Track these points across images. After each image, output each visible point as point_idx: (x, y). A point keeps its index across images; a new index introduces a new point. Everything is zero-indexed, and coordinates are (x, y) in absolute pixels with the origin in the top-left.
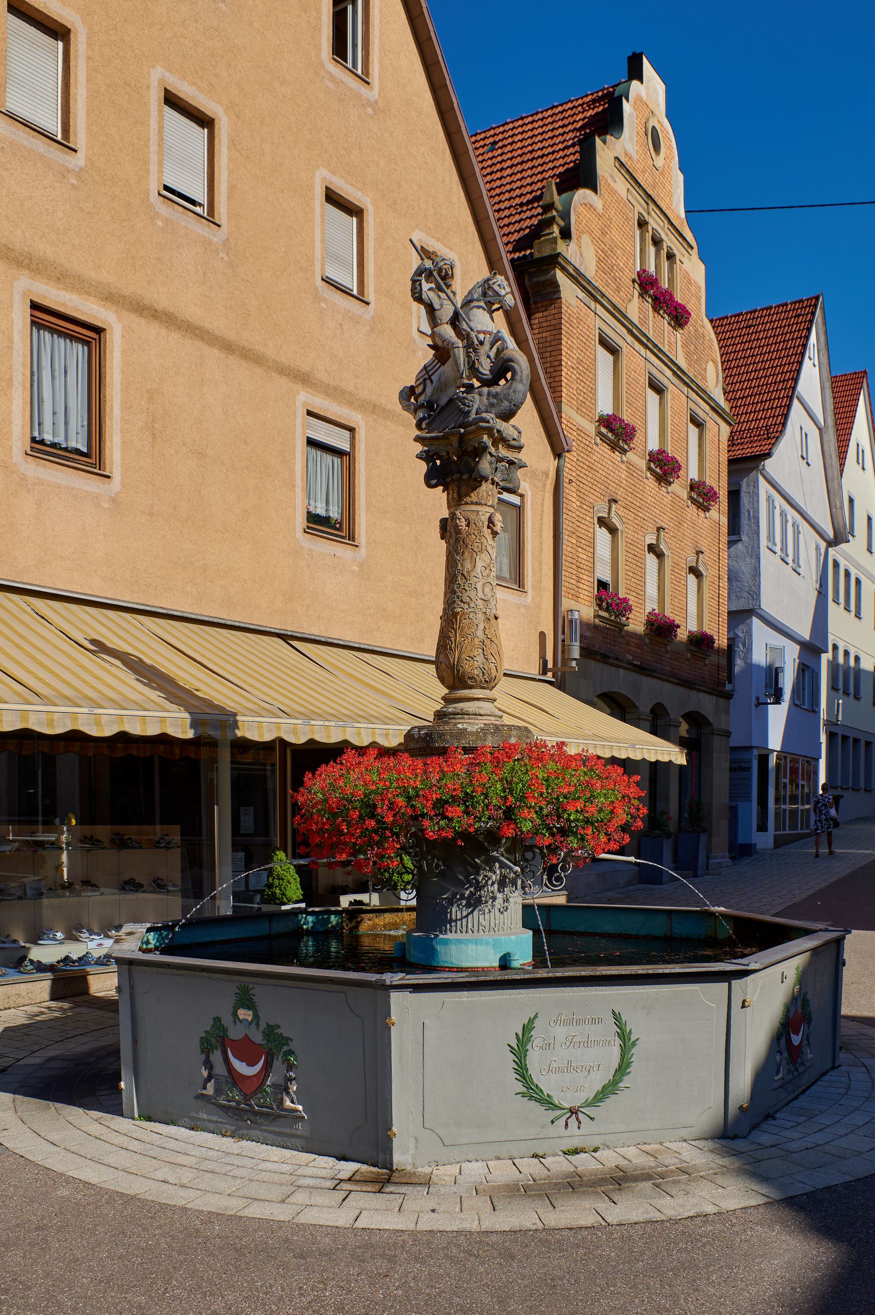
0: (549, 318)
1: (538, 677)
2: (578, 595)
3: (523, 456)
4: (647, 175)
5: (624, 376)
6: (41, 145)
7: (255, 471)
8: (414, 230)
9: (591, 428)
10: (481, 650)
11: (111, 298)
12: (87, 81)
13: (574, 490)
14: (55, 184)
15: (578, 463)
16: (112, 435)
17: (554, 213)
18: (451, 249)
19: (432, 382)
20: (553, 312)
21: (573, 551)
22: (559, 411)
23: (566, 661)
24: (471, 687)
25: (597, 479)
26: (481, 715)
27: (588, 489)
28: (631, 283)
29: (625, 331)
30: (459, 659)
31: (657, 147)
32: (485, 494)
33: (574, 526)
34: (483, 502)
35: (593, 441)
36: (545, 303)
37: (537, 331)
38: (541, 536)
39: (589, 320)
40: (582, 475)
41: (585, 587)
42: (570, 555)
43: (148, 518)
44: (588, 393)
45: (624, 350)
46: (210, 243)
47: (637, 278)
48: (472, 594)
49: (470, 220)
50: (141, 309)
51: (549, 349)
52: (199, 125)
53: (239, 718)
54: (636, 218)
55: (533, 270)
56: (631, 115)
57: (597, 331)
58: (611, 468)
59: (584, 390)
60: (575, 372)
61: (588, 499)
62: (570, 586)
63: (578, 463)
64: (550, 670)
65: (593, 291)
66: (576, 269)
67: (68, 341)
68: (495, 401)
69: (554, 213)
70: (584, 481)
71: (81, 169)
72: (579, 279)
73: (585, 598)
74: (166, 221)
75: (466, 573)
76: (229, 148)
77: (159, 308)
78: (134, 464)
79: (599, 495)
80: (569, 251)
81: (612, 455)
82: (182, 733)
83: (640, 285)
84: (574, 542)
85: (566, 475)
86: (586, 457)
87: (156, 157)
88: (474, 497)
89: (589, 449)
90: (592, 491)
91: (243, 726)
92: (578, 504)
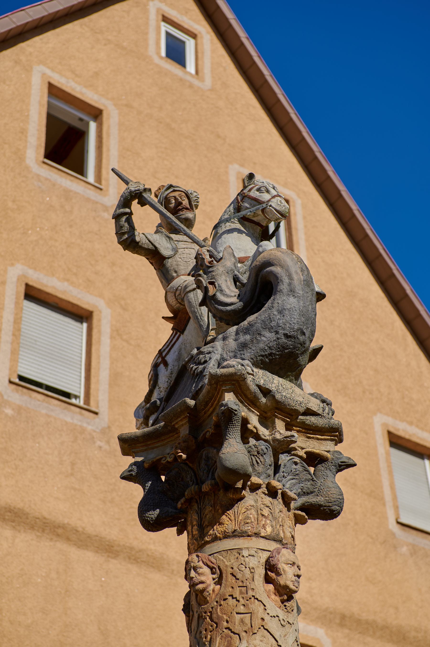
3: (345, 450)
32: (253, 514)
34: (248, 528)
46: (83, 431)
68: (248, 337)
74: (19, 409)
76: (112, 338)
88: (228, 522)
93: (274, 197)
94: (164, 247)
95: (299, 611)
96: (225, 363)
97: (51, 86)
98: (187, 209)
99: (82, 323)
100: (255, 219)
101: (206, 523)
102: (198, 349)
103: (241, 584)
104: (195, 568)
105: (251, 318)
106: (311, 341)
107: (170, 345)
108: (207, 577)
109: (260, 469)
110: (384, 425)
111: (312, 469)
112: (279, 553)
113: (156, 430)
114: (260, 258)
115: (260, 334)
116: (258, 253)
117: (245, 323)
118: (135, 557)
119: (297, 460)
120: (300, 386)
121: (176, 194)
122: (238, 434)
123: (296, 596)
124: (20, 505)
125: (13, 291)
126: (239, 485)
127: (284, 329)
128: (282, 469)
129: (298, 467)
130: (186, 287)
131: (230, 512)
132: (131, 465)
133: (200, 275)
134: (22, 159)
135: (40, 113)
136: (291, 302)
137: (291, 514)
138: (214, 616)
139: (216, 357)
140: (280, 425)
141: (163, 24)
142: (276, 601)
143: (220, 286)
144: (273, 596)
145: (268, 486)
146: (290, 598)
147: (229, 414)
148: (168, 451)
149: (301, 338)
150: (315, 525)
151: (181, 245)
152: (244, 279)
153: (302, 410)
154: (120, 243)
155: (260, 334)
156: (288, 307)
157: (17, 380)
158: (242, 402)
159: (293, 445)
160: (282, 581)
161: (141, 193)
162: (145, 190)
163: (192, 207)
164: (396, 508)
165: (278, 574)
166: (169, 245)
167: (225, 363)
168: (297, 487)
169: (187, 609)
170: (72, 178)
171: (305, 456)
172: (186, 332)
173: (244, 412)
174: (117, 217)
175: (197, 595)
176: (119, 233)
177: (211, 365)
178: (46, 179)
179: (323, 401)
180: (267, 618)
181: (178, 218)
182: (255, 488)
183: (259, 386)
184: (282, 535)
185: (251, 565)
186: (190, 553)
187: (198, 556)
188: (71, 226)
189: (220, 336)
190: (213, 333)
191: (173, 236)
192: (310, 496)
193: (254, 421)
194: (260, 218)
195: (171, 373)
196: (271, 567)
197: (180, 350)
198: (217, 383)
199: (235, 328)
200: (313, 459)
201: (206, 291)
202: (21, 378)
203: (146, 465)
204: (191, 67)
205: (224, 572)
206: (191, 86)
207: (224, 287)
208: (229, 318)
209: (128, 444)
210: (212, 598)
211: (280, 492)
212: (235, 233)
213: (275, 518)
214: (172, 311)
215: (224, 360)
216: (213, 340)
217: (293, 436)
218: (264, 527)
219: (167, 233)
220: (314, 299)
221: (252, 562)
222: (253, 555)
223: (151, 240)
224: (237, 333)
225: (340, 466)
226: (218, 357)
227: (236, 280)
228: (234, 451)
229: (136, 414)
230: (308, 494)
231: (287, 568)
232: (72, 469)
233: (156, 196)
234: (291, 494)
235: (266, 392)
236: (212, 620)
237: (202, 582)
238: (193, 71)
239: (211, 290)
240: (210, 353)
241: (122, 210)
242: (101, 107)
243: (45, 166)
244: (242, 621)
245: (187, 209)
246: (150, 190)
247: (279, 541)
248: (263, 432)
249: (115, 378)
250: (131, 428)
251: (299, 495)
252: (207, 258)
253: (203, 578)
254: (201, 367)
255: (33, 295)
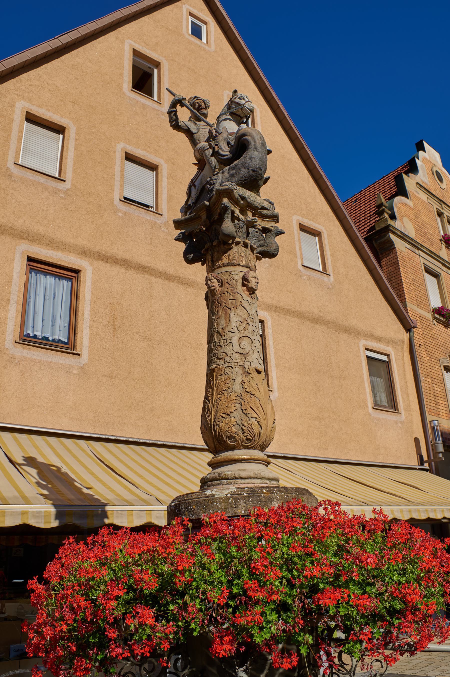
0: (390, 260)
1: (418, 467)
2: (438, 413)
3: (280, 226)
4: (438, 192)
5: (445, 288)
6: (41, 178)
7: (191, 348)
8: (294, 215)
9: (429, 316)
10: (238, 406)
11: (85, 253)
12: (75, 149)
13: (424, 350)
14: (50, 197)
15: (424, 335)
16: (82, 330)
17: (383, 207)
18: (319, 224)
19: (195, 186)
20: (392, 256)
21: (430, 386)
22: (405, 307)
23: (436, 453)
24: (233, 448)
25: (439, 344)
26: (242, 478)
27: (434, 350)
28: (439, 241)
29: (440, 265)
30: (215, 417)
31: (441, 180)
32: (237, 255)
33: (428, 371)
34: (234, 262)
35: (432, 323)
36: (387, 253)
37: (385, 268)
38: (405, 378)
39: (416, 259)
40: (428, 342)
41: (442, 408)
42: (428, 389)
43: (109, 379)
44: (423, 297)
45: (442, 274)
46: (155, 223)
47: (442, 239)
48: (227, 349)
49: (330, 210)
50: (106, 258)
51: (393, 276)
52: (150, 170)
53: (108, 508)
54: (435, 210)
55: (377, 237)
56: (421, 165)
57: (423, 265)
58: (447, 338)
59: (420, 295)
60: (412, 285)
61: (434, 355)
62: (432, 408)
63: (424, 335)
64: (426, 462)
65: (415, 244)
66: (401, 232)
67: (57, 279)
68: (234, 171)
69: (383, 207)
70: (429, 345)
71: (68, 189)
72: (405, 238)
73: (444, 414)
74: (125, 213)
75: (220, 330)
76: (168, 178)
77: (119, 257)
78: (99, 346)
79: (442, 353)
80: (397, 224)
81: (446, 330)
82: (45, 523)
83: (445, 242)
84: (430, 381)
85: (416, 342)
86: (428, 332)
87: (119, 183)
88: (225, 259)
89: (430, 327)
90: (436, 351)
91: (112, 514)
92: (428, 358)
93: (247, 102)
94: (193, 128)
95: (257, 298)
96: (224, 184)
97: (134, 50)
98: (204, 108)
99: (153, 171)
100: (238, 113)
101: (215, 260)
102: (210, 178)
103: (231, 287)
104: (210, 280)
105: (236, 162)
106: (265, 173)
107: (196, 177)
108: (216, 284)
109: (240, 234)
110: (298, 220)
111: (264, 235)
112: (249, 273)
113: (191, 217)
114: (240, 132)
115: (240, 170)
116: (239, 130)
117: (233, 164)
118: (182, 281)
119: (257, 230)
120: (259, 196)
121: (198, 101)
122: (230, 218)
123: (256, 292)
124: (128, 258)
125: (119, 156)
126: (230, 242)
127: (252, 167)
128: (250, 235)
129: (258, 234)
130: (204, 148)
131: (226, 255)
132: (179, 234)
133: (211, 141)
134: (121, 89)
135: (129, 65)
136: (255, 154)
137: (254, 256)
138: (219, 301)
139: (219, 181)
140: (249, 214)
141: (190, 17)
142: (247, 294)
143: (220, 147)
144: (246, 292)
145: (244, 242)
146: (254, 293)
147: (226, 208)
148: (196, 227)
149: (260, 172)
150: (266, 260)
151: (201, 127)
152: (232, 143)
153: (260, 207)
154: (171, 126)
155: (240, 170)
156: (254, 156)
157: (123, 200)
158: (231, 203)
159: (255, 224)
160: (250, 285)
161: (181, 100)
162: (183, 99)
163: (206, 108)
164: (302, 259)
165: (248, 282)
166: (195, 127)
167: (224, 184)
168: (257, 243)
169: (207, 298)
170: (146, 98)
171: (261, 229)
172: (204, 171)
173: (233, 208)
174: (169, 113)
175: (211, 292)
176: (171, 121)
177: (217, 185)
178: (134, 99)
179: (270, 203)
180: (243, 301)
181: (200, 113)
182: (238, 243)
183: (239, 195)
184: (250, 265)
185: (236, 279)
186: (208, 274)
187: (211, 275)
188: (146, 123)
189: (221, 171)
190: (217, 170)
191: (197, 122)
192: (263, 247)
193: (237, 212)
194: (240, 113)
195: (198, 190)
196: (245, 279)
197: (202, 179)
198: (219, 194)
199: (228, 167)
200: (265, 230)
201: (214, 149)
202: (125, 198)
203: (186, 234)
204: (204, 40)
205: (223, 282)
206: (204, 50)
207: (223, 147)
208: (225, 162)
209: (178, 224)
210: (218, 293)
211: (249, 245)
212: (228, 121)
213: (247, 257)
214: (197, 160)
215: (223, 183)
216: (217, 173)
217: (256, 219)
218: (242, 261)
219: (194, 121)
220: (266, 153)
221: (236, 277)
222: (237, 273)
223: (187, 124)
224: (229, 170)
225: (277, 233)
226: (220, 181)
227: (228, 143)
228: (228, 226)
229: (181, 211)
230: (262, 246)
231: (252, 279)
232: (151, 241)
233: (189, 102)
234: (255, 246)
235: (243, 198)
236: (218, 303)
237: (214, 286)
238: (205, 42)
239: (216, 149)
240: (216, 179)
241: (172, 109)
242: (160, 61)
243: (133, 92)
244: (232, 303)
245: (204, 108)
246: (185, 99)
247: (248, 267)
248: (242, 217)
249: (170, 198)
250: (179, 216)
251: (258, 247)
252: (214, 132)
253: (214, 284)
254: (212, 186)
255: (129, 158)
